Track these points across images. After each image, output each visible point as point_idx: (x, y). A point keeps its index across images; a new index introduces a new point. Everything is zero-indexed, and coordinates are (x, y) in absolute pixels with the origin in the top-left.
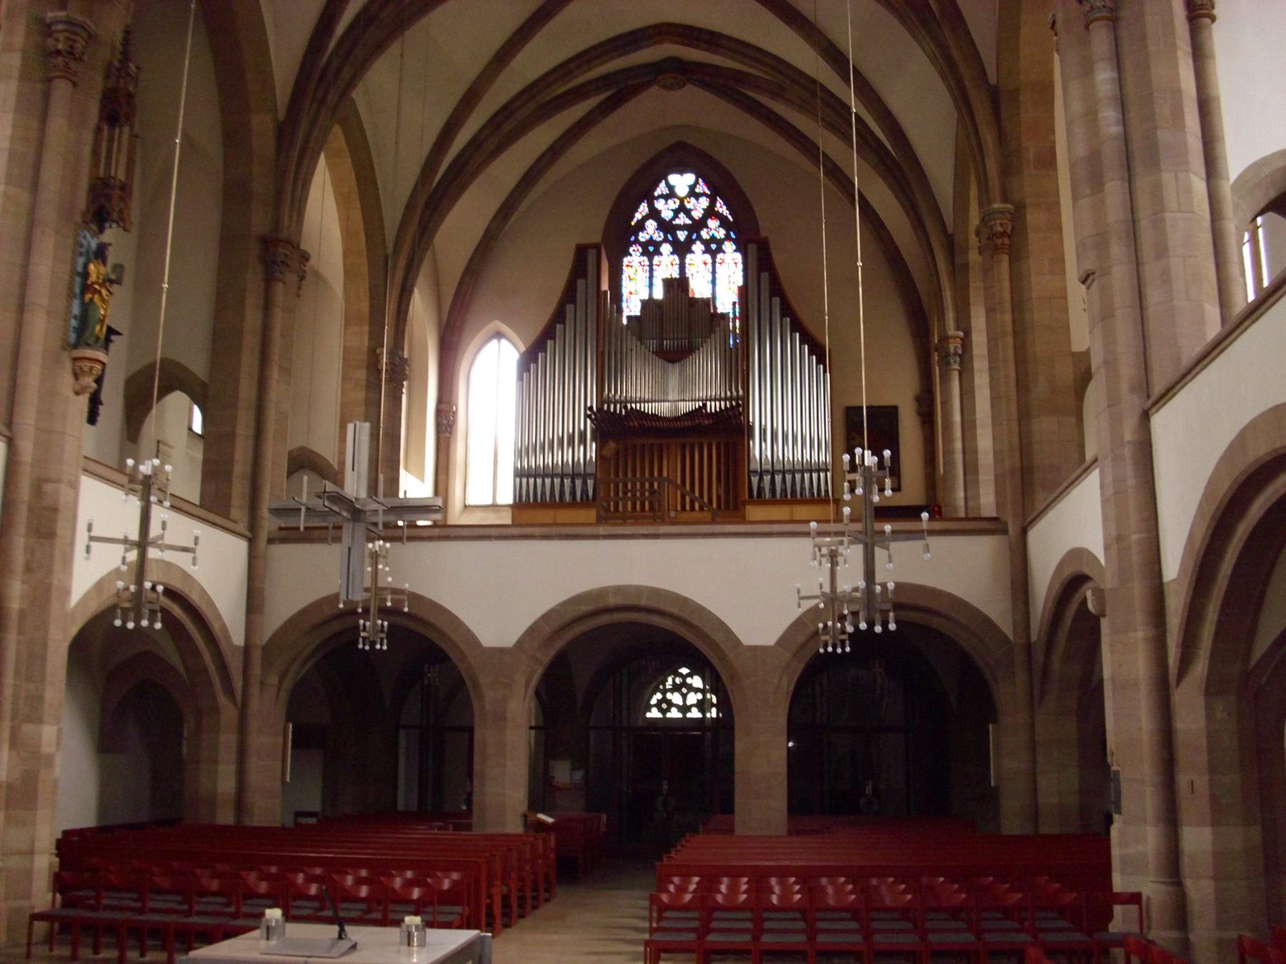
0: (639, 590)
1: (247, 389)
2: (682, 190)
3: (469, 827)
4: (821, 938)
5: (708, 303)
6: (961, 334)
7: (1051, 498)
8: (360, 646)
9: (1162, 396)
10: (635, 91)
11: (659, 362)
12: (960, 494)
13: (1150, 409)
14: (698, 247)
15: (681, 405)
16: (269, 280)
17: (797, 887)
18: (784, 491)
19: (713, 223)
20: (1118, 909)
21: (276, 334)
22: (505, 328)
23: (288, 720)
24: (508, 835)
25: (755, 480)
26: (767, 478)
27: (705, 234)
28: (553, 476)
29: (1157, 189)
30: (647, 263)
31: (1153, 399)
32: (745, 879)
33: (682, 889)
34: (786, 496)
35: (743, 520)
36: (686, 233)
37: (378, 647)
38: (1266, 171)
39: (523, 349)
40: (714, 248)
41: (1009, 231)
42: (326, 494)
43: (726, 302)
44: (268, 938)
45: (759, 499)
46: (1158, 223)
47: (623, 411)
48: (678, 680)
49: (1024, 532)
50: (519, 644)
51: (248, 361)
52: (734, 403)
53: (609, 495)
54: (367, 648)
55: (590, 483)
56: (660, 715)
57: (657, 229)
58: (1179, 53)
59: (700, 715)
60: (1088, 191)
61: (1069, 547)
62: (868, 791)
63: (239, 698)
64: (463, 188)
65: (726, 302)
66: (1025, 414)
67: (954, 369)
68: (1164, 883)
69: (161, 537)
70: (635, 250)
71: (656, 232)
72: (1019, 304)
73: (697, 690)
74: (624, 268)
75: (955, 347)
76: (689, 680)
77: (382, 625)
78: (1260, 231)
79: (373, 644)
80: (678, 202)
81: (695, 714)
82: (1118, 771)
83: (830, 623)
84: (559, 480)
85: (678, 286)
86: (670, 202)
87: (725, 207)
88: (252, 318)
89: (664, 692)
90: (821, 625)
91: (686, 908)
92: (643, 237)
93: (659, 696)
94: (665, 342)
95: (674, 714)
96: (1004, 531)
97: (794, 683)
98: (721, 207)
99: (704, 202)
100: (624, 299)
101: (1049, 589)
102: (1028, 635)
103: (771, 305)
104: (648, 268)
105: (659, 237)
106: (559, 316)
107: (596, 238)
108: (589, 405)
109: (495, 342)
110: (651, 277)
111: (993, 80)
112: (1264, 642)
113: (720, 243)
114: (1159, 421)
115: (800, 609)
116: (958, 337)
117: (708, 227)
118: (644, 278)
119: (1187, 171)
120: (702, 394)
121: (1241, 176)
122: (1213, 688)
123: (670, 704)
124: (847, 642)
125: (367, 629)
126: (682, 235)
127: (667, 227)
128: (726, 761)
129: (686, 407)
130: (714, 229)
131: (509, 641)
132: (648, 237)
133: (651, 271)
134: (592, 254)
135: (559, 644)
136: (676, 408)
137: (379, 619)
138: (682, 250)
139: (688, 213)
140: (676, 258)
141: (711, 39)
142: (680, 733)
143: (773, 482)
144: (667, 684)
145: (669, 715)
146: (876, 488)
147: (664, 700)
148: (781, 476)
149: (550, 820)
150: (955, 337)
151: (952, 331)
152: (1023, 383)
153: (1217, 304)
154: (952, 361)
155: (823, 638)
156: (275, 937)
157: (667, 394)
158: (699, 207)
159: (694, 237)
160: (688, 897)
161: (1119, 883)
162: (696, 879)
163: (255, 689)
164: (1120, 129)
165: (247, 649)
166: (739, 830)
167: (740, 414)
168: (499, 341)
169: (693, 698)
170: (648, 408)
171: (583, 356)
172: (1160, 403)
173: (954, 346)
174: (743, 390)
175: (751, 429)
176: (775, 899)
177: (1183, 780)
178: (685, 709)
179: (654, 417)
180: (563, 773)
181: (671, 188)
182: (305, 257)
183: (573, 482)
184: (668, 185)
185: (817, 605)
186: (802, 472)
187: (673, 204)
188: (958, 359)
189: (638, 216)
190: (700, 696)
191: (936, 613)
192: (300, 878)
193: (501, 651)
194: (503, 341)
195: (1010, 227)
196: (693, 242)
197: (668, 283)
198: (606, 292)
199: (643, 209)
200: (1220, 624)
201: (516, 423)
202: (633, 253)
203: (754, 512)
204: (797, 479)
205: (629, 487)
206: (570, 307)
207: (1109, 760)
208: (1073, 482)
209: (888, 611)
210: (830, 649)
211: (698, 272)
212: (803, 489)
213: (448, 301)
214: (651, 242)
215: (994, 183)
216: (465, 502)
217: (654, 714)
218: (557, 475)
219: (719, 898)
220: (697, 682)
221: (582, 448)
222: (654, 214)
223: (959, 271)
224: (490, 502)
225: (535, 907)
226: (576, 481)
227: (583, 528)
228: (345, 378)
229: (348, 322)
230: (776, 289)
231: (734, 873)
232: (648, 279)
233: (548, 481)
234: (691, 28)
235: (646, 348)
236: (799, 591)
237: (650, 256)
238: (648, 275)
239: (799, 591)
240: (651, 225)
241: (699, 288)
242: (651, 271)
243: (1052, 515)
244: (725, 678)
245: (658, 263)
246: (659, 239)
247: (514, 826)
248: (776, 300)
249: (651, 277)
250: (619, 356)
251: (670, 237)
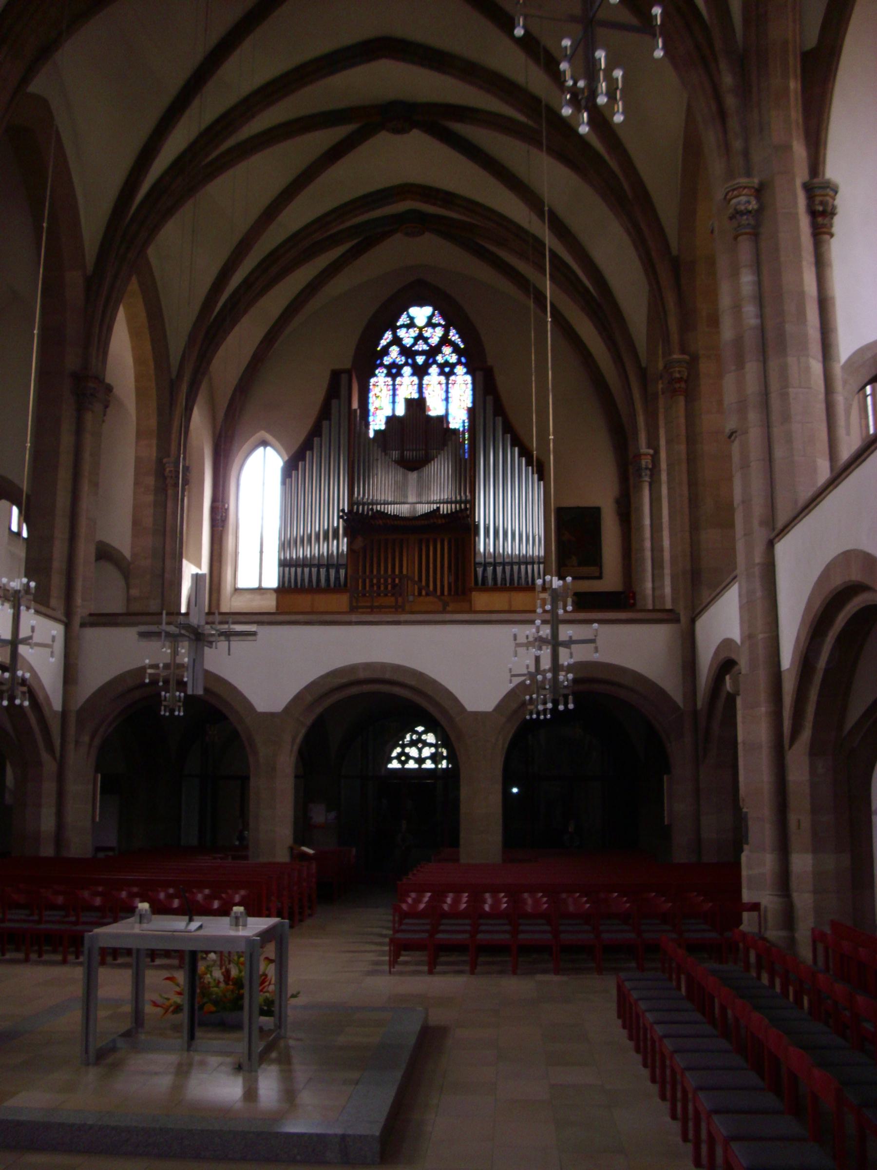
0: (383, 666)
1: (62, 500)
2: (421, 321)
3: (246, 858)
4: (521, 936)
5: (443, 420)
6: (651, 452)
7: (713, 595)
8: (162, 713)
9: (782, 531)
10: (385, 236)
11: (401, 470)
12: (649, 585)
13: (774, 538)
14: (434, 370)
15: (419, 506)
16: (80, 410)
17: (505, 899)
18: (504, 579)
19: (447, 350)
20: (745, 915)
21: (87, 456)
22: (269, 437)
23: (97, 771)
24: (278, 863)
25: (480, 570)
26: (490, 569)
27: (440, 359)
28: (311, 566)
29: (784, 371)
30: (391, 383)
31: (776, 531)
32: (467, 894)
33: (417, 901)
34: (506, 584)
35: (471, 611)
36: (424, 357)
37: (176, 713)
38: (869, 355)
39: (286, 458)
40: (447, 370)
41: (685, 377)
42: (182, 625)
43: (458, 420)
44: (140, 922)
45: (483, 587)
46: (784, 396)
47: (370, 513)
48: (414, 737)
49: (693, 621)
50: (287, 709)
51: (64, 475)
52: (463, 506)
53: (358, 588)
54: (167, 714)
55: (342, 572)
56: (399, 766)
57: (399, 354)
58: (804, 263)
59: (433, 766)
60: (733, 368)
61: (719, 641)
62: (571, 829)
63: (58, 755)
64: (234, 323)
65: (458, 420)
66: (695, 527)
67: (646, 481)
68: (776, 895)
69: (31, 638)
70: (381, 373)
71: (399, 356)
72: (692, 439)
73: (430, 745)
74: (371, 387)
75: (647, 462)
76: (424, 737)
77: (180, 696)
78: (869, 399)
79: (172, 711)
80: (417, 331)
81: (429, 765)
82: (747, 812)
83: (534, 696)
84: (316, 569)
85: (417, 405)
86: (411, 330)
87: (457, 336)
88: (67, 440)
89: (403, 746)
90: (528, 697)
91: (422, 915)
92: (387, 360)
93: (399, 750)
94: (405, 452)
95: (411, 765)
96: (677, 621)
97: (508, 743)
98: (454, 336)
99: (439, 332)
100: (371, 414)
101: (710, 670)
102: (695, 704)
103: (494, 423)
104: (391, 387)
105: (401, 360)
106: (316, 431)
107: (348, 365)
108: (341, 508)
109: (261, 449)
110: (394, 395)
111: (675, 252)
112: (855, 714)
113: (453, 366)
114: (780, 548)
115: (511, 685)
116: (649, 454)
117: (443, 354)
118: (388, 395)
119: (808, 356)
120: (435, 497)
121: (850, 359)
122: (815, 750)
123: (408, 757)
124: (571, 698)
125: (167, 699)
126: (420, 360)
127: (407, 352)
128: (453, 805)
129: (423, 509)
130: (448, 355)
131: (278, 706)
132: (391, 360)
133: (394, 390)
134: (344, 378)
135: (319, 710)
136: (414, 509)
137: (177, 690)
138: (420, 372)
139: (426, 340)
140: (415, 380)
141: (447, 198)
142: (416, 781)
143: (495, 571)
144: (405, 740)
145: (407, 766)
146: (561, 604)
147: (403, 753)
148: (501, 567)
149: (311, 851)
150: (646, 455)
151: (644, 449)
152: (694, 501)
153: (828, 457)
154: (643, 474)
155: (530, 707)
156: (145, 921)
157: (406, 496)
158: (435, 335)
159: (431, 361)
160: (422, 906)
161: (747, 896)
162: (429, 894)
163: (71, 746)
164: (758, 321)
165: (64, 713)
166: (464, 860)
167: (468, 516)
168: (265, 448)
169: (427, 752)
170: (391, 509)
171: (337, 464)
172: (781, 536)
173: (646, 462)
174: (471, 495)
175: (477, 527)
176: (487, 908)
177: (793, 818)
178: (420, 761)
179: (396, 517)
180: (320, 815)
181: (412, 319)
182: (109, 389)
183: (328, 571)
184: (409, 316)
185: (524, 681)
186: (519, 564)
187: (414, 332)
188: (648, 472)
189: (383, 342)
190: (433, 750)
191: (620, 686)
192: (124, 894)
193: (272, 715)
194: (269, 449)
195: (686, 374)
196: (430, 366)
197: (409, 402)
198: (355, 410)
199: (388, 336)
200: (818, 703)
201: (281, 517)
202: (379, 375)
203: (481, 600)
204: (515, 570)
205: (375, 581)
206: (325, 424)
207: (741, 804)
208: (724, 588)
209: (569, 695)
210: (534, 716)
211: (433, 391)
212: (519, 578)
213: (221, 414)
214: (393, 365)
215: (675, 337)
216: (235, 585)
217: (395, 765)
218: (314, 565)
219: (446, 907)
220: (430, 738)
221: (335, 542)
222: (397, 341)
223: (650, 400)
224: (255, 585)
225: (301, 921)
226: (331, 570)
227: (339, 616)
228: (137, 483)
229: (140, 434)
230: (499, 410)
231: (458, 890)
232: (391, 397)
233: (307, 570)
234: (430, 189)
235: (390, 458)
236: (510, 670)
237: (394, 377)
238: (391, 393)
239: (510, 670)
240: (394, 350)
241: (435, 408)
242: (394, 390)
243: (713, 610)
244: (453, 738)
245: (400, 383)
246: (400, 363)
247: (282, 856)
248: (499, 420)
249: (394, 395)
250: (367, 464)
251: (410, 361)
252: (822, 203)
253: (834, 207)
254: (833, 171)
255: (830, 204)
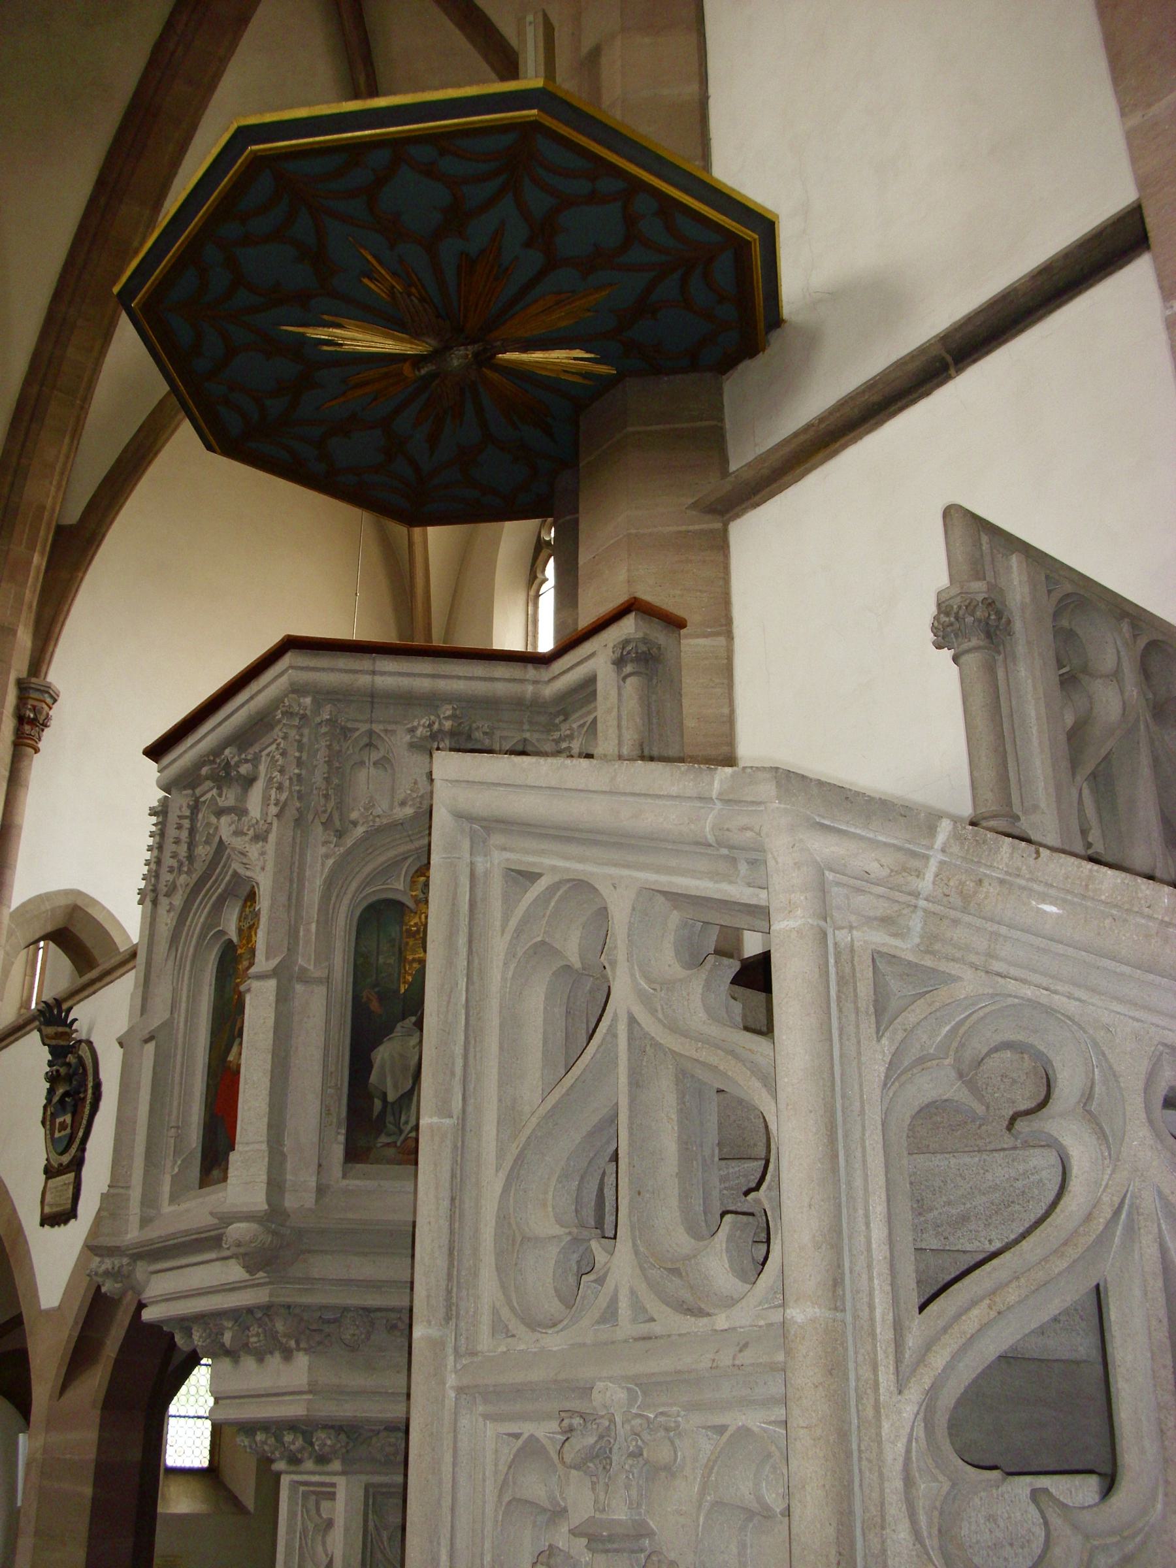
78: (41, 952)
121: (23, 905)
252: (34, 708)
253: (48, 717)
254: (57, 675)
255: (44, 713)
